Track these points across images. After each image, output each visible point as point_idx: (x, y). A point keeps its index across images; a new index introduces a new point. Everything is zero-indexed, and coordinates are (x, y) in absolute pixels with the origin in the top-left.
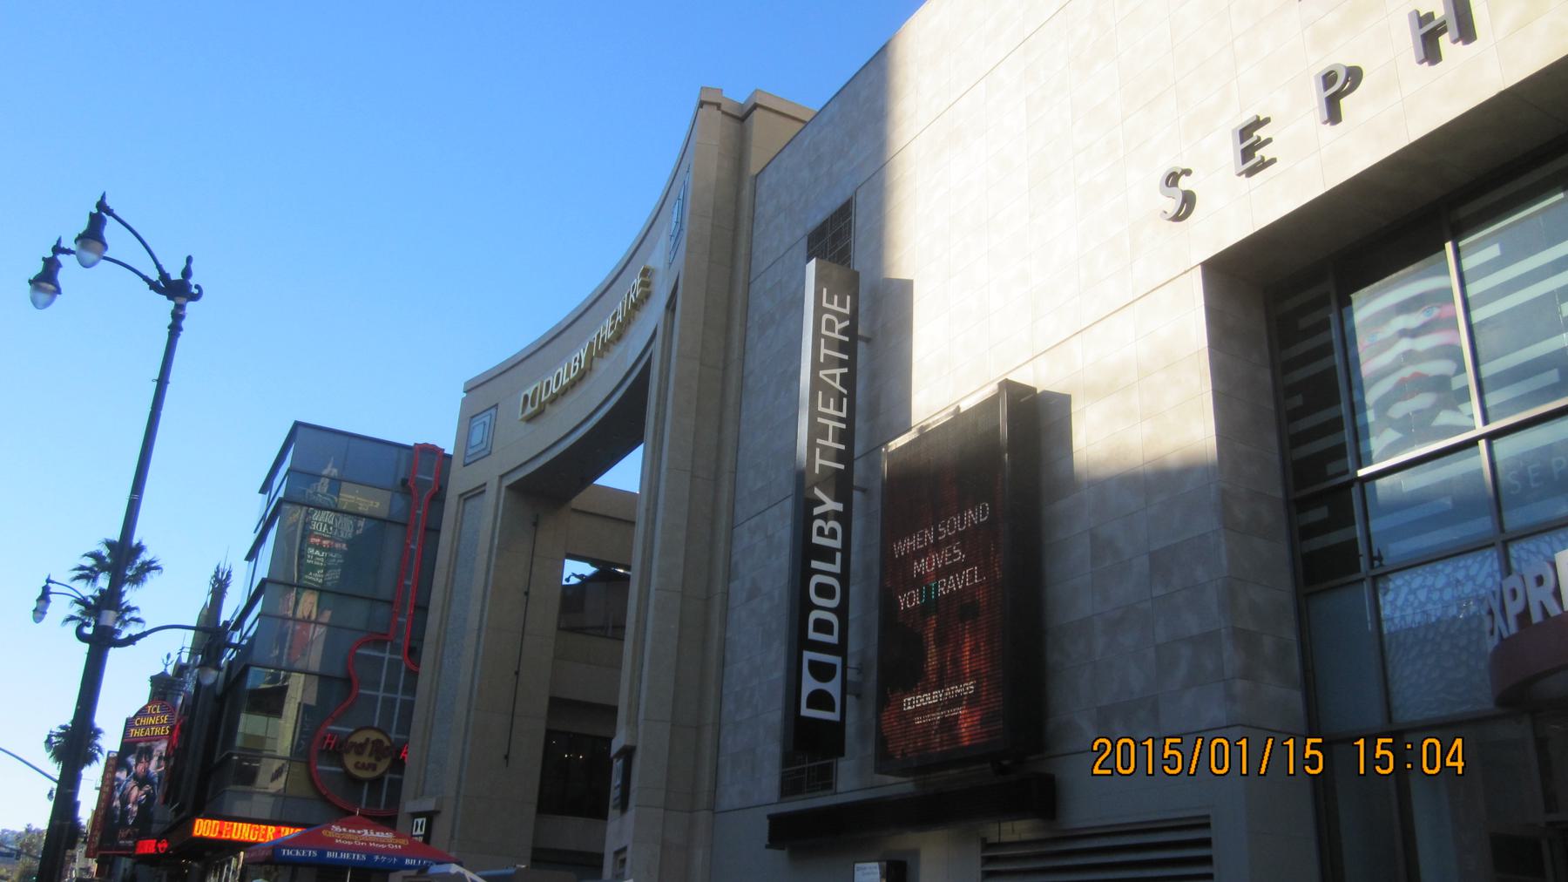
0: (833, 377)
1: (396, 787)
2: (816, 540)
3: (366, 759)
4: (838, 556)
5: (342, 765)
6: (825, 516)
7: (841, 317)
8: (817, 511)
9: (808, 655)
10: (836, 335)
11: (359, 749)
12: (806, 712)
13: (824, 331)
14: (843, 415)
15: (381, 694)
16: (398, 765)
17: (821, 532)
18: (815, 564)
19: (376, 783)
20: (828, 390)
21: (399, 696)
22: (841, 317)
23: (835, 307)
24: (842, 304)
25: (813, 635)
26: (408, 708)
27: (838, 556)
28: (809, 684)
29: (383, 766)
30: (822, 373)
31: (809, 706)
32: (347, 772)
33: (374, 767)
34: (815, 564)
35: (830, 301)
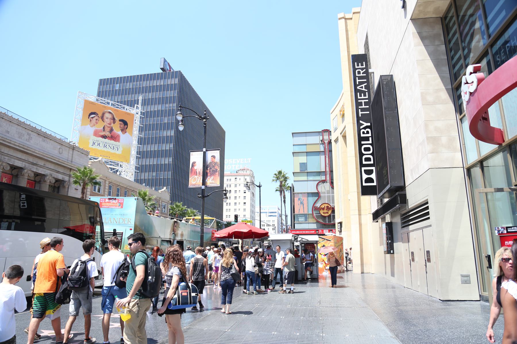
0: (362, 87)
1: (334, 216)
2: (362, 135)
3: (325, 211)
4: (370, 138)
5: (320, 213)
6: (365, 128)
7: (362, 69)
8: (361, 127)
9: (363, 169)
10: (361, 75)
11: (323, 209)
12: (364, 184)
13: (357, 75)
14: (367, 97)
15: (326, 195)
16: (333, 211)
17: (364, 133)
18: (363, 142)
19: (329, 216)
20: (361, 92)
21: (331, 195)
22: (362, 69)
23: (360, 67)
24: (362, 65)
25: (364, 163)
26: (333, 197)
27: (370, 138)
28: (22, 204)
29: (330, 212)
30: (358, 88)
31: (365, 182)
32: (322, 215)
33: (327, 213)
34: (363, 142)
35: (358, 65)
